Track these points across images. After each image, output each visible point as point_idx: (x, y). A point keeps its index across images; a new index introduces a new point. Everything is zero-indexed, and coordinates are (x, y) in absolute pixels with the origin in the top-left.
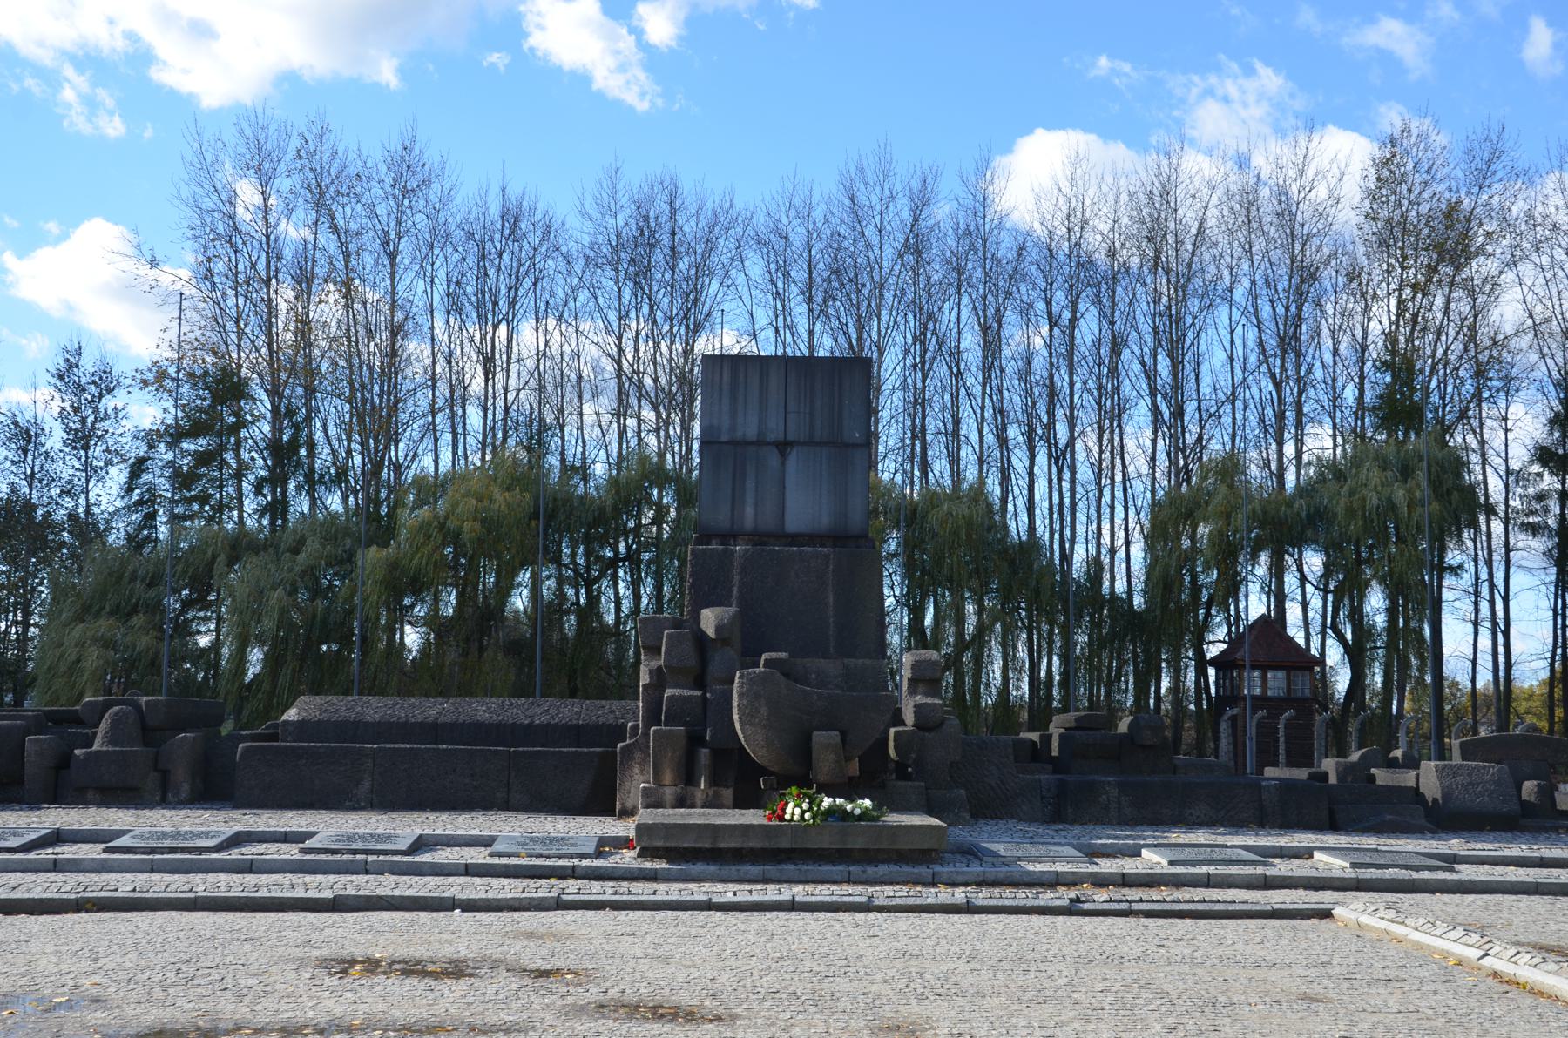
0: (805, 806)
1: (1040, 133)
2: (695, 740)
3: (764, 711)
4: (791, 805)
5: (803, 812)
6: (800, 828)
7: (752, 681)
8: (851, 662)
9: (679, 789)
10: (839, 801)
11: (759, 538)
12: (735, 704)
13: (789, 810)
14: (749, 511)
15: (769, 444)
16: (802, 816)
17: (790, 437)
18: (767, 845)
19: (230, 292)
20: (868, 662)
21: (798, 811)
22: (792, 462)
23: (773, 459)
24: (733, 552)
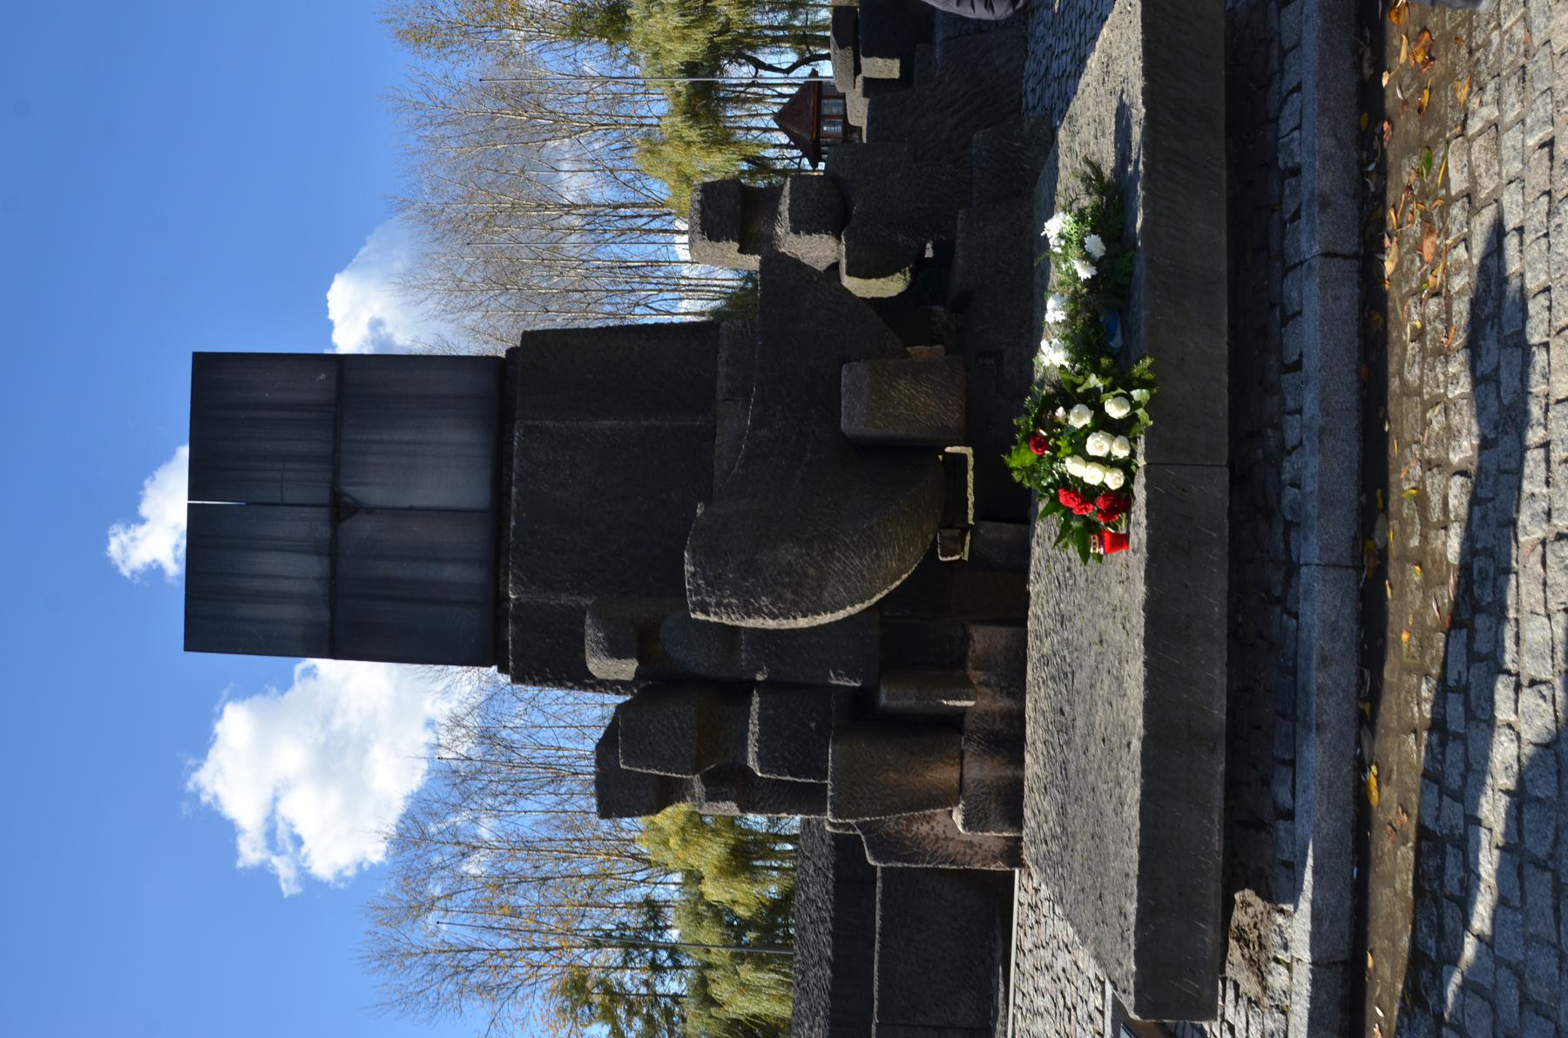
0: (1080, 418)
1: (330, 295)
2: (860, 713)
3: (788, 554)
4: (1074, 467)
5: (1103, 423)
6: (1167, 444)
7: (715, 584)
8: (722, 385)
9: (970, 749)
10: (1054, 312)
11: (496, 558)
12: (771, 624)
13: (1093, 475)
14: (450, 572)
15: (335, 536)
16: (1114, 428)
17: (324, 495)
18: (1217, 555)
19: (514, 972)
20: (723, 355)
21: (1097, 445)
22: (374, 495)
23: (362, 528)
24: (519, 605)
